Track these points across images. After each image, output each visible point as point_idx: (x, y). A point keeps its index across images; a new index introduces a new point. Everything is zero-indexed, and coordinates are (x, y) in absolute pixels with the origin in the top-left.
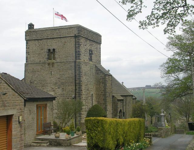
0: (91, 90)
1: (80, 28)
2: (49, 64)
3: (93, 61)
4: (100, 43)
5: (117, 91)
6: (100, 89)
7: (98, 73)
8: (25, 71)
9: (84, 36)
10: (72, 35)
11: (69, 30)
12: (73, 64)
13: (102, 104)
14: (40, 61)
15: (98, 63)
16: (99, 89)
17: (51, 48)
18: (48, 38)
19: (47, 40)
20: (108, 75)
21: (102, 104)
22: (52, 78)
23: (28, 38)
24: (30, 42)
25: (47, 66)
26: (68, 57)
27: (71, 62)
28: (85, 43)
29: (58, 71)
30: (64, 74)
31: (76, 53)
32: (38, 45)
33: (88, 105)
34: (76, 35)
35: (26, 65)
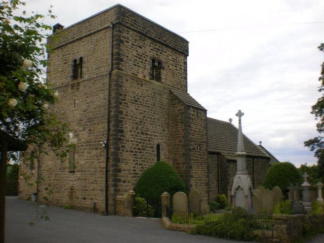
0: (155, 136)
1: (121, 12)
2: (73, 86)
4: (185, 53)
9: (132, 27)
10: (107, 26)
11: (103, 16)
12: (107, 80)
15: (179, 89)
18: (74, 39)
19: (73, 44)
20: (193, 107)
22: (75, 112)
25: (70, 90)
30: (92, 102)
32: (61, 56)
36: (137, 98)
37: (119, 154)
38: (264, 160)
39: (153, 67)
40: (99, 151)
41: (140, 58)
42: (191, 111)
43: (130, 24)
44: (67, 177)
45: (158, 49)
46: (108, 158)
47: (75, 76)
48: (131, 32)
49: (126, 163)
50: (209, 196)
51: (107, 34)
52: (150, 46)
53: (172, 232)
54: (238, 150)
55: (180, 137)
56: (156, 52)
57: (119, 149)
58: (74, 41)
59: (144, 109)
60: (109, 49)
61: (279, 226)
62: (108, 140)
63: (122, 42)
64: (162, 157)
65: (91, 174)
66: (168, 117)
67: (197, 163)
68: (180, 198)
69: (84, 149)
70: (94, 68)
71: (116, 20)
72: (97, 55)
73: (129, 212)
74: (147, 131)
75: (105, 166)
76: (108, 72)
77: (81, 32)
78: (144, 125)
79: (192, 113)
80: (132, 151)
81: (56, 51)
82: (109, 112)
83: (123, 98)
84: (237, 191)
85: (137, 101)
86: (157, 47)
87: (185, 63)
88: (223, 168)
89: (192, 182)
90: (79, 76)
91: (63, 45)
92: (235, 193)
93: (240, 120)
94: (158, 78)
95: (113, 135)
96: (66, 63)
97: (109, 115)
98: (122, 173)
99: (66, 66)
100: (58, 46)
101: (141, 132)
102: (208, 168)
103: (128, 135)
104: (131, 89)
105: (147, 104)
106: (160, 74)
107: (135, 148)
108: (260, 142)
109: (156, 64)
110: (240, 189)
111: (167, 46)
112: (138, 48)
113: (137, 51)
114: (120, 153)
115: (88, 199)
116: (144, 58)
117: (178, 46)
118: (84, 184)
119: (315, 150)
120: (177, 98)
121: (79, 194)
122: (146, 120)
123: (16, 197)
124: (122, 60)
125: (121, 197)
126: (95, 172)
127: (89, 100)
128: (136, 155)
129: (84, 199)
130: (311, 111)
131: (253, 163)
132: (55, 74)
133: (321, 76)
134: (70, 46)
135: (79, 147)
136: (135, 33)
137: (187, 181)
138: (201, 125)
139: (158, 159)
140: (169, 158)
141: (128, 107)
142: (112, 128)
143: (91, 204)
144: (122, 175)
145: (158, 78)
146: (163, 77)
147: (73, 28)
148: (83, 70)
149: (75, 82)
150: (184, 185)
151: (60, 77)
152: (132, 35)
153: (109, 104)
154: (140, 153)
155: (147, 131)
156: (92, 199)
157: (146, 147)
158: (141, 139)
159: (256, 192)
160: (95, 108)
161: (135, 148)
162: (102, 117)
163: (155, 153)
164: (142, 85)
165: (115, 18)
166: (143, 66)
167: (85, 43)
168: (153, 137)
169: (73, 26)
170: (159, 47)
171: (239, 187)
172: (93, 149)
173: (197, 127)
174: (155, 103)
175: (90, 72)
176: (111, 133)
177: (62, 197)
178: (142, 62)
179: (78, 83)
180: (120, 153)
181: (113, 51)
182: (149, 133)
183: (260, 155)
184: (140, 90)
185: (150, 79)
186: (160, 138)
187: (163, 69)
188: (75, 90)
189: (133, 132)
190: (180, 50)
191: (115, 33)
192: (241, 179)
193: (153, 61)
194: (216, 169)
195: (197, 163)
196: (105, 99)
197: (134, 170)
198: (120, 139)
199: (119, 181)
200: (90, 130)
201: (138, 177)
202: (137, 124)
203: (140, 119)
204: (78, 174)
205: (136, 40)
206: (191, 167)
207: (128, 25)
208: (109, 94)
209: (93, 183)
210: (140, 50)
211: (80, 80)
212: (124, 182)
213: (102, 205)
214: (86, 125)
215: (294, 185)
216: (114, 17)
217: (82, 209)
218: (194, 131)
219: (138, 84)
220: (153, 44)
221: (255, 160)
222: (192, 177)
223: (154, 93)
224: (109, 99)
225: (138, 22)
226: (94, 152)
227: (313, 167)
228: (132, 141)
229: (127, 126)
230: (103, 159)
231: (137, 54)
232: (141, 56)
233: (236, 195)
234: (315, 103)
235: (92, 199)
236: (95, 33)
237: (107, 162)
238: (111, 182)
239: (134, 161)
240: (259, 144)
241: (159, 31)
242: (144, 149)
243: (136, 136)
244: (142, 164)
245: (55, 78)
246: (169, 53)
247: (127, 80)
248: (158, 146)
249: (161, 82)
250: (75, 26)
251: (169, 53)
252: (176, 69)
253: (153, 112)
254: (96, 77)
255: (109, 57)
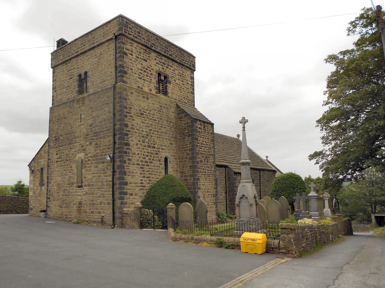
0: (162, 149)
1: (122, 22)
3: (170, 95)
4: (192, 68)
5: (235, 159)
6: (185, 148)
7: (181, 118)
8: (50, 120)
9: (136, 40)
10: (109, 38)
11: (105, 28)
13: (188, 176)
14: (68, 99)
15: (186, 103)
16: (183, 148)
17: (82, 73)
19: (77, 58)
20: (200, 121)
21: (188, 176)
22: (82, 127)
23: (55, 64)
24: (57, 71)
26: (105, 81)
27: (108, 90)
28: (142, 55)
29: (90, 111)
30: (98, 116)
31: (116, 70)
32: (66, 72)
33: (151, 176)
34: (116, 34)
35: (52, 109)
36: (143, 112)
37: (125, 167)
38: (270, 173)
39: (159, 81)
40: (105, 164)
41: (145, 71)
42: (198, 125)
43: (134, 36)
44: (76, 192)
45: (163, 63)
46: (114, 172)
47: (81, 91)
48: (135, 45)
49: (133, 176)
50: (216, 207)
51: (110, 46)
52: (155, 59)
53: (232, 250)
54: (242, 158)
55: (187, 150)
56: (162, 65)
57: (125, 162)
58: (78, 56)
59: (150, 122)
60: (113, 62)
61: (285, 236)
62: (114, 153)
63: (126, 54)
64: (170, 170)
65: (98, 188)
66: (176, 131)
67: (205, 175)
68: (186, 208)
69: (91, 163)
70: (99, 82)
71: (118, 31)
72: (100, 68)
73: (136, 224)
74: (154, 144)
75: (111, 179)
76: (112, 86)
77: (84, 46)
78: (151, 139)
79: (199, 126)
80: (138, 164)
81: (61, 66)
82: (114, 125)
83: (128, 111)
84: (241, 200)
85: (143, 114)
86: (163, 61)
87: (192, 78)
88: (231, 178)
89: (200, 194)
90: (85, 91)
91: (67, 61)
92: (239, 202)
93: (244, 127)
94: (165, 93)
95: (118, 148)
96: (71, 78)
97: (114, 129)
98: (128, 187)
99: (71, 81)
100: (63, 61)
101: (148, 145)
102: (216, 180)
103: (134, 149)
104: (136, 102)
105: (153, 117)
106: (166, 88)
107: (141, 161)
108: (267, 157)
109: (163, 78)
110: (244, 198)
111: (173, 60)
112: (143, 61)
113: (142, 64)
114: (126, 166)
115: (96, 213)
116: (149, 72)
117: (186, 62)
118: (92, 198)
119: (320, 163)
120: (183, 112)
121: (86, 208)
122: (153, 133)
123: (28, 215)
124: (126, 73)
125: (127, 209)
126: (102, 186)
127: (95, 114)
128: (143, 168)
129: (92, 212)
130: (326, 58)
131: (260, 176)
132: (61, 89)
133: (326, 90)
134: (74, 60)
135: (86, 161)
136: (140, 46)
137: (194, 193)
138: (208, 139)
139: (166, 172)
140: (177, 171)
141: (133, 120)
142: (117, 141)
143: (99, 218)
144: (128, 188)
145: (165, 93)
146: (169, 91)
147: (76, 42)
148: (88, 84)
149: (81, 96)
150: (191, 196)
151: (66, 92)
152: (136, 48)
153: (114, 118)
154: (148, 166)
155: (154, 144)
156: (99, 213)
157: (153, 160)
158: (148, 152)
159: (264, 202)
160: (101, 122)
161: (141, 161)
162: (107, 130)
163: (163, 166)
164: (147, 99)
165: (117, 30)
166: (148, 80)
167: (89, 57)
168: (160, 150)
169: (76, 40)
170: (165, 61)
171: (243, 195)
172: (99, 163)
173: (202, 139)
174: (162, 116)
175: (95, 86)
176: (117, 146)
177: (70, 212)
178: (147, 76)
179: (84, 97)
180: (126, 166)
181: (116, 63)
182: (156, 146)
183: (266, 168)
184: (145, 105)
185: (156, 93)
186: (168, 151)
187: (170, 83)
188: (81, 105)
189: (139, 145)
190: (186, 65)
191: (118, 45)
192: (247, 188)
193: (159, 75)
194: (224, 181)
195: (205, 175)
196: (110, 112)
197: (142, 183)
198: (126, 152)
199: (126, 194)
200: (96, 144)
201: (146, 189)
202: (143, 137)
203: (147, 132)
204: (86, 189)
205: (140, 53)
206: (198, 179)
207: (131, 37)
208: (114, 107)
209: (100, 197)
210: (145, 64)
211: (85, 95)
212: (131, 195)
213: (109, 218)
214: (92, 139)
215: (301, 195)
216: (117, 28)
217: (89, 222)
218: (202, 144)
219: (144, 97)
220: (158, 58)
221: (262, 172)
222: (200, 189)
223: (161, 106)
224: (114, 112)
225: (142, 35)
226: (101, 166)
227: (318, 179)
228: (138, 154)
229: (133, 139)
230: (110, 172)
231: (141, 69)
232: (147, 69)
233: (241, 204)
234: (320, 116)
235: (99, 213)
236: (98, 46)
237: (113, 175)
238: (117, 195)
239: (141, 174)
240: (266, 159)
241: (164, 45)
242: (152, 162)
243: (143, 149)
244: (149, 177)
245: (61, 94)
246: (176, 68)
247: (132, 93)
248: (166, 159)
249: (167, 96)
250: (78, 40)
251: (176, 68)
252: (183, 84)
253: (160, 125)
254: (101, 91)
255: (113, 70)
